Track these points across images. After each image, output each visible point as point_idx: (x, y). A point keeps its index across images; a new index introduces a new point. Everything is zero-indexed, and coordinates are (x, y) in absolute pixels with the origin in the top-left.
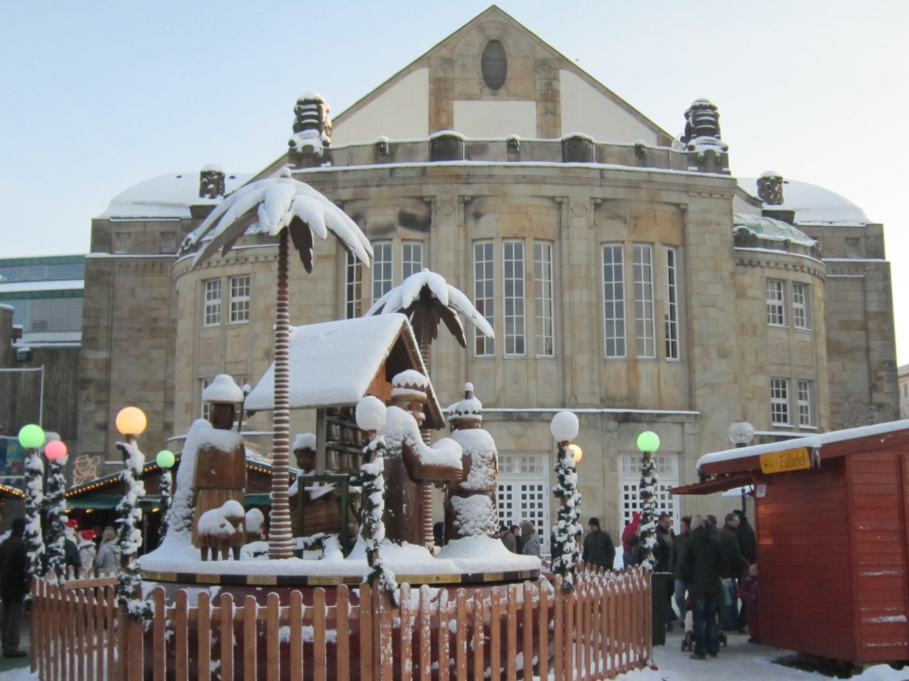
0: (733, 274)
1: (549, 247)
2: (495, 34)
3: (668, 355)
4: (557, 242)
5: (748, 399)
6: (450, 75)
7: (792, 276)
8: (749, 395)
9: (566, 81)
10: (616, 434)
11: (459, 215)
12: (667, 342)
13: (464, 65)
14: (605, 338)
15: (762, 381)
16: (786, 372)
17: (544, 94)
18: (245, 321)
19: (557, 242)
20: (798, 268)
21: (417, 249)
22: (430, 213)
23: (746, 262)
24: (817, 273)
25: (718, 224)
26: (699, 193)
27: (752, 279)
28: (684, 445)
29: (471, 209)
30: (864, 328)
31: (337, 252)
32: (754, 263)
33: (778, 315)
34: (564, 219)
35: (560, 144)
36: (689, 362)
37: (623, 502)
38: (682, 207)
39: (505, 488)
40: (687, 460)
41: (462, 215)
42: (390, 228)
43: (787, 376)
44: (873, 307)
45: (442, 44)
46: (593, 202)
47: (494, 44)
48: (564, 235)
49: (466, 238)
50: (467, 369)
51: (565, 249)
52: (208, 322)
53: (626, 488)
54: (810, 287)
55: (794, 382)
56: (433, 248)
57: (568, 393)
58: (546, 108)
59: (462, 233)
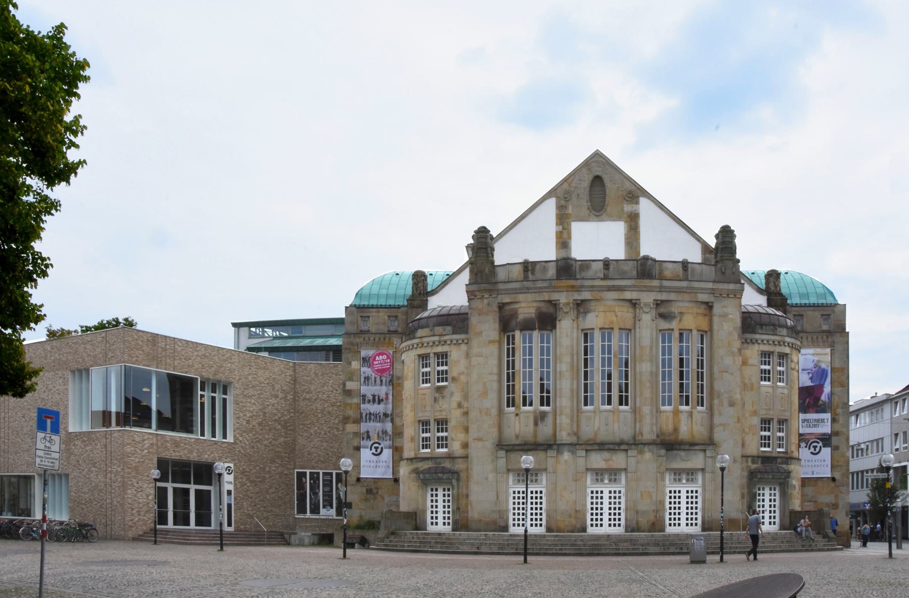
0: (740, 350)
2: (598, 171)
3: (698, 405)
4: (633, 331)
7: (778, 349)
9: (644, 207)
10: (665, 458)
11: (573, 314)
12: (698, 384)
14: (661, 370)
15: (756, 421)
16: (771, 414)
20: (782, 343)
24: (794, 346)
26: (721, 295)
27: (753, 353)
31: (500, 338)
33: (765, 375)
34: (638, 315)
36: (711, 409)
37: (668, 500)
38: (710, 304)
40: (707, 474)
41: (575, 312)
43: (771, 417)
45: (565, 180)
46: (655, 302)
47: (598, 180)
48: (637, 326)
50: (577, 416)
51: (638, 335)
54: (789, 356)
55: (775, 421)
56: (558, 336)
59: (575, 325)
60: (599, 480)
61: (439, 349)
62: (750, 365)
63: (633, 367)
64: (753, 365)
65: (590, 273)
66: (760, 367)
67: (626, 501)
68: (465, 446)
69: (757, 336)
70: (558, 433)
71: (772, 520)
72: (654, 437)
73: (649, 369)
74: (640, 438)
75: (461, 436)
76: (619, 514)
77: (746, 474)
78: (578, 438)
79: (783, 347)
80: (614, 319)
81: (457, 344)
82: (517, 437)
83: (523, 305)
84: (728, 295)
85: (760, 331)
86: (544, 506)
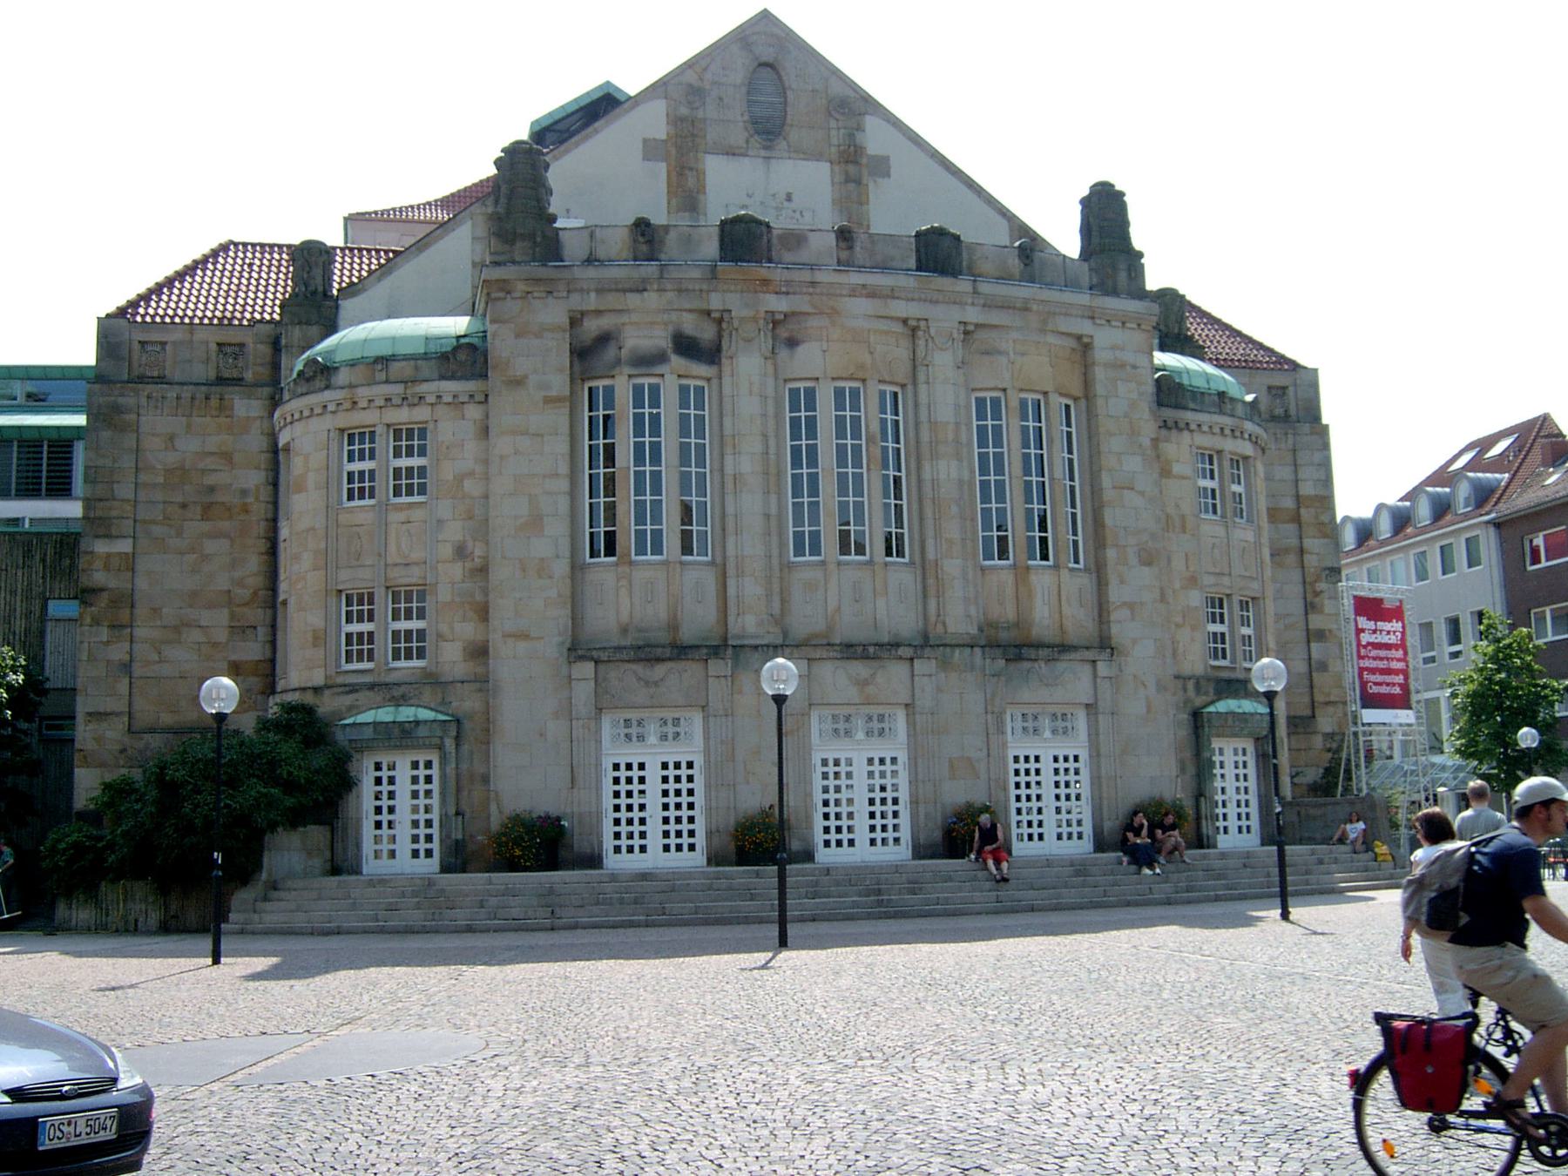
0: (1155, 441)
1: (1067, 407)
2: (767, 54)
4: (910, 387)
5: (1178, 626)
6: (700, 114)
7: (1229, 445)
8: (1179, 619)
11: (765, 343)
13: (721, 99)
14: (791, 530)
15: (1195, 599)
17: (844, 151)
18: (416, 499)
19: (910, 387)
20: (1238, 434)
21: (700, 391)
22: (720, 337)
23: (1170, 423)
25: (1134, 367)
27: (1180, 450)
28: (913, 695)
29: (783, 333)
30: (1296, 519)
32: (1182, 425)
34: (921, 352)
35: (913, 240)
38: (1085, 340)
39: (635, 767)
40: (1101, 717)
42: (659, 358)
44: (1307, 489)
46: (962, 328)
48: (921, 377)
49: (776, 378)
51: (923, 399)
52: (350, 498)
53: (825, 762)
54: (1251, 460)
56: (727, 390)
57: (933, 619)
58: (847, 173)
59: (770, 369)
60: (634, 739)
61: (401, 416)
62: (1175, 477)
63: (913, 465)
64: (1183, 478)
65: (804, 256)
66: (1196, 483)
67: (708, 786)
68: (480, 652)
69: (1189, 416)
70: (731, 619)
71: (1244, 823)
72: (974, 631)
73: (954, 475)
74: (940, 629)
75: (468, 630)
76: (691, 820)
77: (1184, 716)
78: (785, 634)
79: (1239, 441)
80: (867, 359)
81: (457, 404)
82: (624, 630)
83: (635, 318)
84: (1123, 323)
85: (1192, 405)
86: (698, 800)
